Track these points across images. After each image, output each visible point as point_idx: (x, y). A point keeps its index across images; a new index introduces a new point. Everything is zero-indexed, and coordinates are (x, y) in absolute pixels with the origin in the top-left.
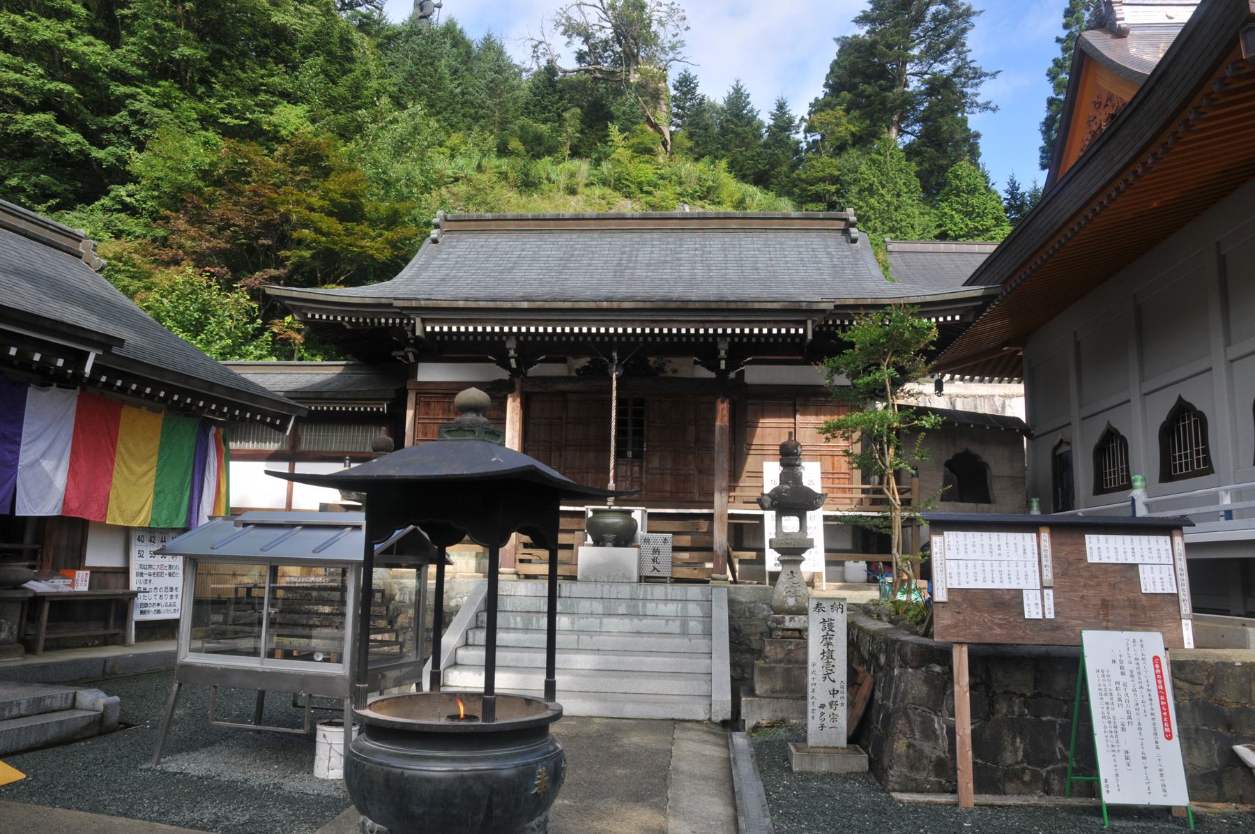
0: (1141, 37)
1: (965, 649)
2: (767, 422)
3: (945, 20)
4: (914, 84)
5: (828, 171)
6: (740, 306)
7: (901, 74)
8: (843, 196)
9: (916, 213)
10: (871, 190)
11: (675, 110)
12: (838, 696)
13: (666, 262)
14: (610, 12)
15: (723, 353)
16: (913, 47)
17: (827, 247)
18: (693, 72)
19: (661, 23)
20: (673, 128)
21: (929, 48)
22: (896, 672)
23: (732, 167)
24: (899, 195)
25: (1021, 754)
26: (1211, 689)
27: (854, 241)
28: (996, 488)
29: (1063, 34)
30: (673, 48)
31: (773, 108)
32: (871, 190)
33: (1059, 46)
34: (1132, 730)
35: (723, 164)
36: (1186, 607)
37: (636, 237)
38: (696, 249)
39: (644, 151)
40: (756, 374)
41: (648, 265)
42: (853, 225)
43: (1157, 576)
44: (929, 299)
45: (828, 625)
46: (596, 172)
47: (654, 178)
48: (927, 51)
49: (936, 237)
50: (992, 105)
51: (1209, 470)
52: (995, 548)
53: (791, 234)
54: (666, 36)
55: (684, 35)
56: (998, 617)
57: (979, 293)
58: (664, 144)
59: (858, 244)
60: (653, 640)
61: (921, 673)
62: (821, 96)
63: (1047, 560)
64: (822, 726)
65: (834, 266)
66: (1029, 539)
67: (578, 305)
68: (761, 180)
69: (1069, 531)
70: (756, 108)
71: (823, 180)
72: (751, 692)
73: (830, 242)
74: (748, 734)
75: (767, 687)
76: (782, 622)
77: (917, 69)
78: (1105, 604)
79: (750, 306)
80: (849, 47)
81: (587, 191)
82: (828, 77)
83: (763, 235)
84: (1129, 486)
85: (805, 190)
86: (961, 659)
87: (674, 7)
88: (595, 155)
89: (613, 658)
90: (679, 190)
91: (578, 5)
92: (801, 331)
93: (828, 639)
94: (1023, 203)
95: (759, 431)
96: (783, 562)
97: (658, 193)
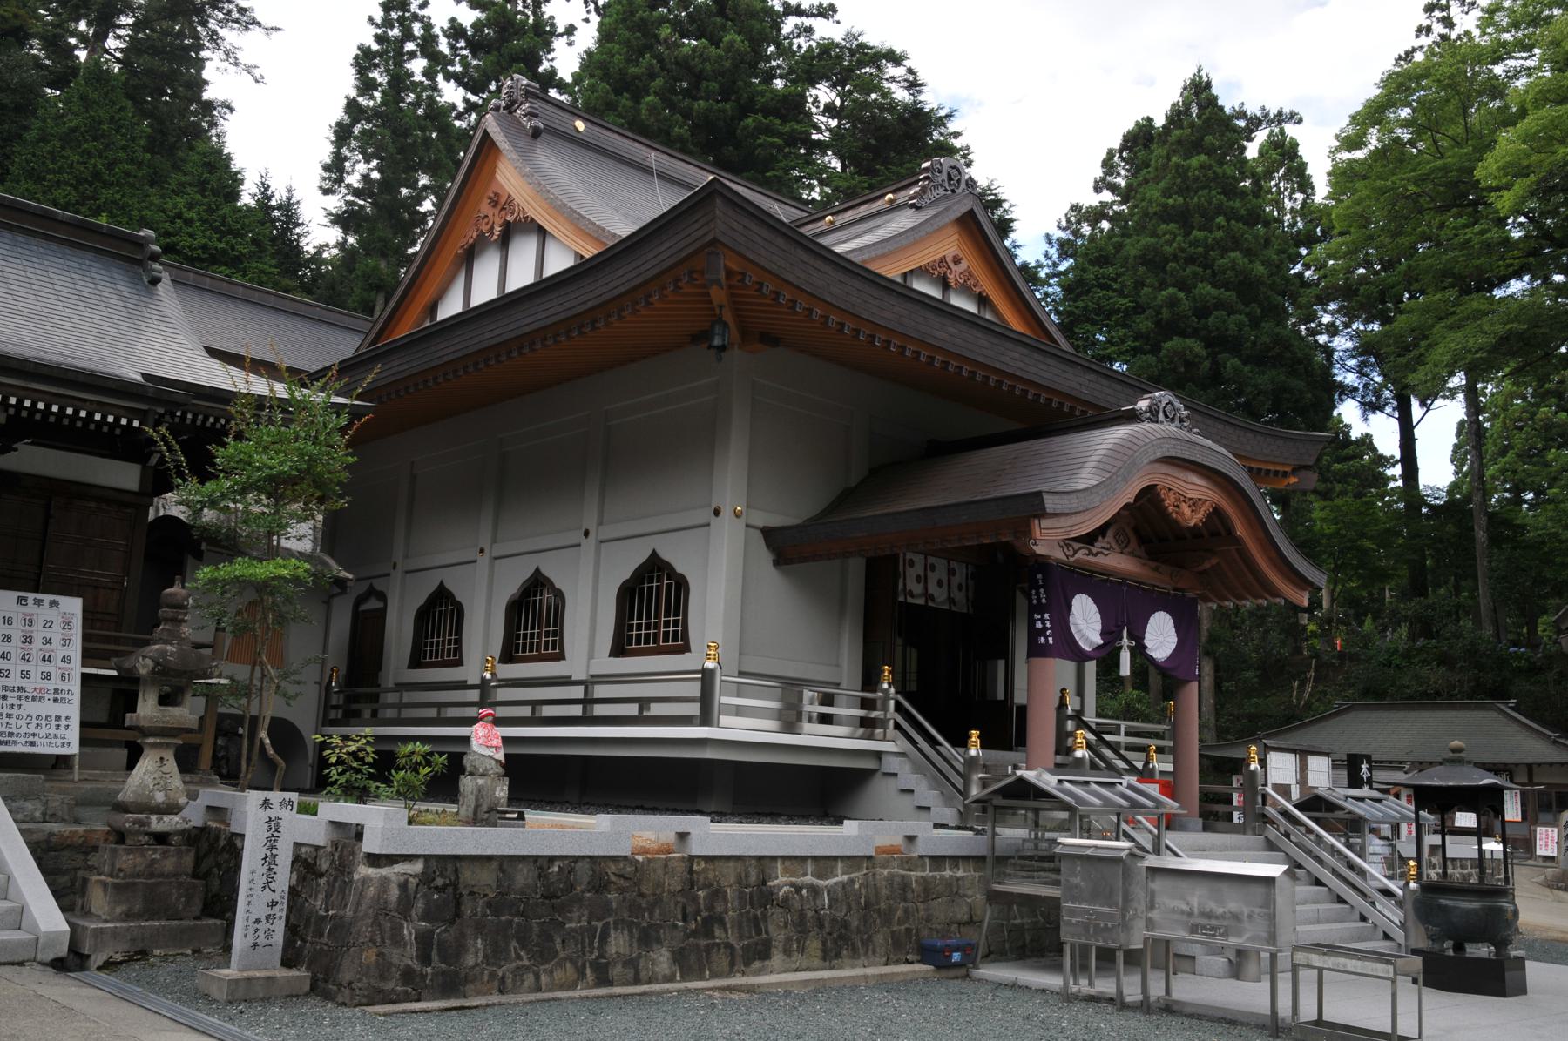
12: (276, 908)
25: (481, 954)
50: (257, 73)
64: (255, 945)
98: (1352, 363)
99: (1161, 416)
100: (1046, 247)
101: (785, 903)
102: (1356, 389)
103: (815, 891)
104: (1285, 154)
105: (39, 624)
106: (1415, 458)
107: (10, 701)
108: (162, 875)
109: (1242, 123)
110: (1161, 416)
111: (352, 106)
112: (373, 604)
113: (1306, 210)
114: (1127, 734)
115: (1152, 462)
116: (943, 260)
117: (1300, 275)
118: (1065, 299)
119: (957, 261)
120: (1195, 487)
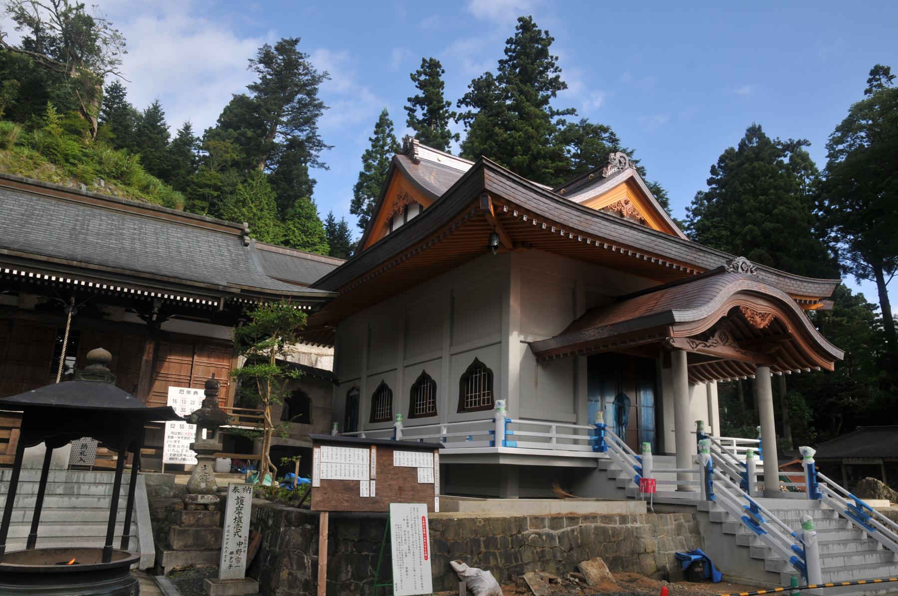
0: (426, 167)
1: (327, 515)
2: (174, 358)
3: (305, 105)
4: (279, 139)
5: (213, 181)
6: (177, 281)
7: (273, 131)
8: (221, 201)
9: (270, 223)
10: (244, 203)
11: (104, 107)
13: (112, 234)
14: (62, 18)
15: (156, 310)
16: (284, 116)
17: (228, 245)
18: (123, 84)
19: (105, 42)
20: (100, 120)
21: (293, 119)
22: (282, 529)
23: (142, 161)
24: (262, 210)
25: (350, 574)
26: (443, 533)
27: (246, 245)
28: (315, 414)
29: (374, 137)
30: (111, 63)
31: (181, 128)
32: (244, 203)
33: (370, 143)
34: (410, 556)
35: (137, 157)
36: (437, 490)
37: (88, 211)
38: (135, 229)
39: (74, 131)
40: (172, 325)
41: (98, 234)
42: (247, 234)
43: (426, 474)
44: (295, 294)
45: (240, 501)
46: (27, 136)
47: (80, 154)
48: (292, 120)
49: (282, 242)
50: (326, 166)
51: (435, 414)
52: (348, 456)
53: (204, 232)
54: (107, 51)
55: (121, 56)
56: (346, 496)
57: (325, 295)
58: (92, 131)
59: (248, 247)
60: (88, 513)
61: (299, 530)
62: (214, 127)
63: (374, 465)
64: (231, 566)
65: (233, 260)
66: (365, 452)
67: (51, 260)
68: (164, 175)
69: (386, 447)
70: (168, 123)
71: (209, 186)
72: (169, 547)
73: (230, 242)
74: (167, 576)
75: (181, 543)
76: (196, 499)
77: (283, 130)
78: (400, 489)
79: (184, 282)
80: (239, 101)
81: (17, 149)
82: (221, 116)
83: (185, 229)
84: (390, 418)
85: (195, 190)
86: (324, 520)
87: (118, 34)
88: (28, 123)
89: (57, 528)
90: (98, 167)
91: (33, 3)
92: (216, 304)
93: (239, 510)
94: (335, 230)
95: (166, 364)
96: (199, 459)
97: (81, 166)
98: (849, 255)
99: (740, 270)
100: (686, 212)
101: (533, 544)
102: (852, 268)
103: (551, 537)
104: (802, 162)
105: (188, 402)
106: (888, 301)
107: (174, 439)
108: (203, 526)
109: (780, 147)
110: (740, 270)
111: (362, 174)
112: (354, 393)
113: (817, 183)
114: (738, 445)
115: (735, 294)
116: (619, 203)
117: (816, 215)
118: (698, 235)
119: (627, 203)
120: (762, 306)
